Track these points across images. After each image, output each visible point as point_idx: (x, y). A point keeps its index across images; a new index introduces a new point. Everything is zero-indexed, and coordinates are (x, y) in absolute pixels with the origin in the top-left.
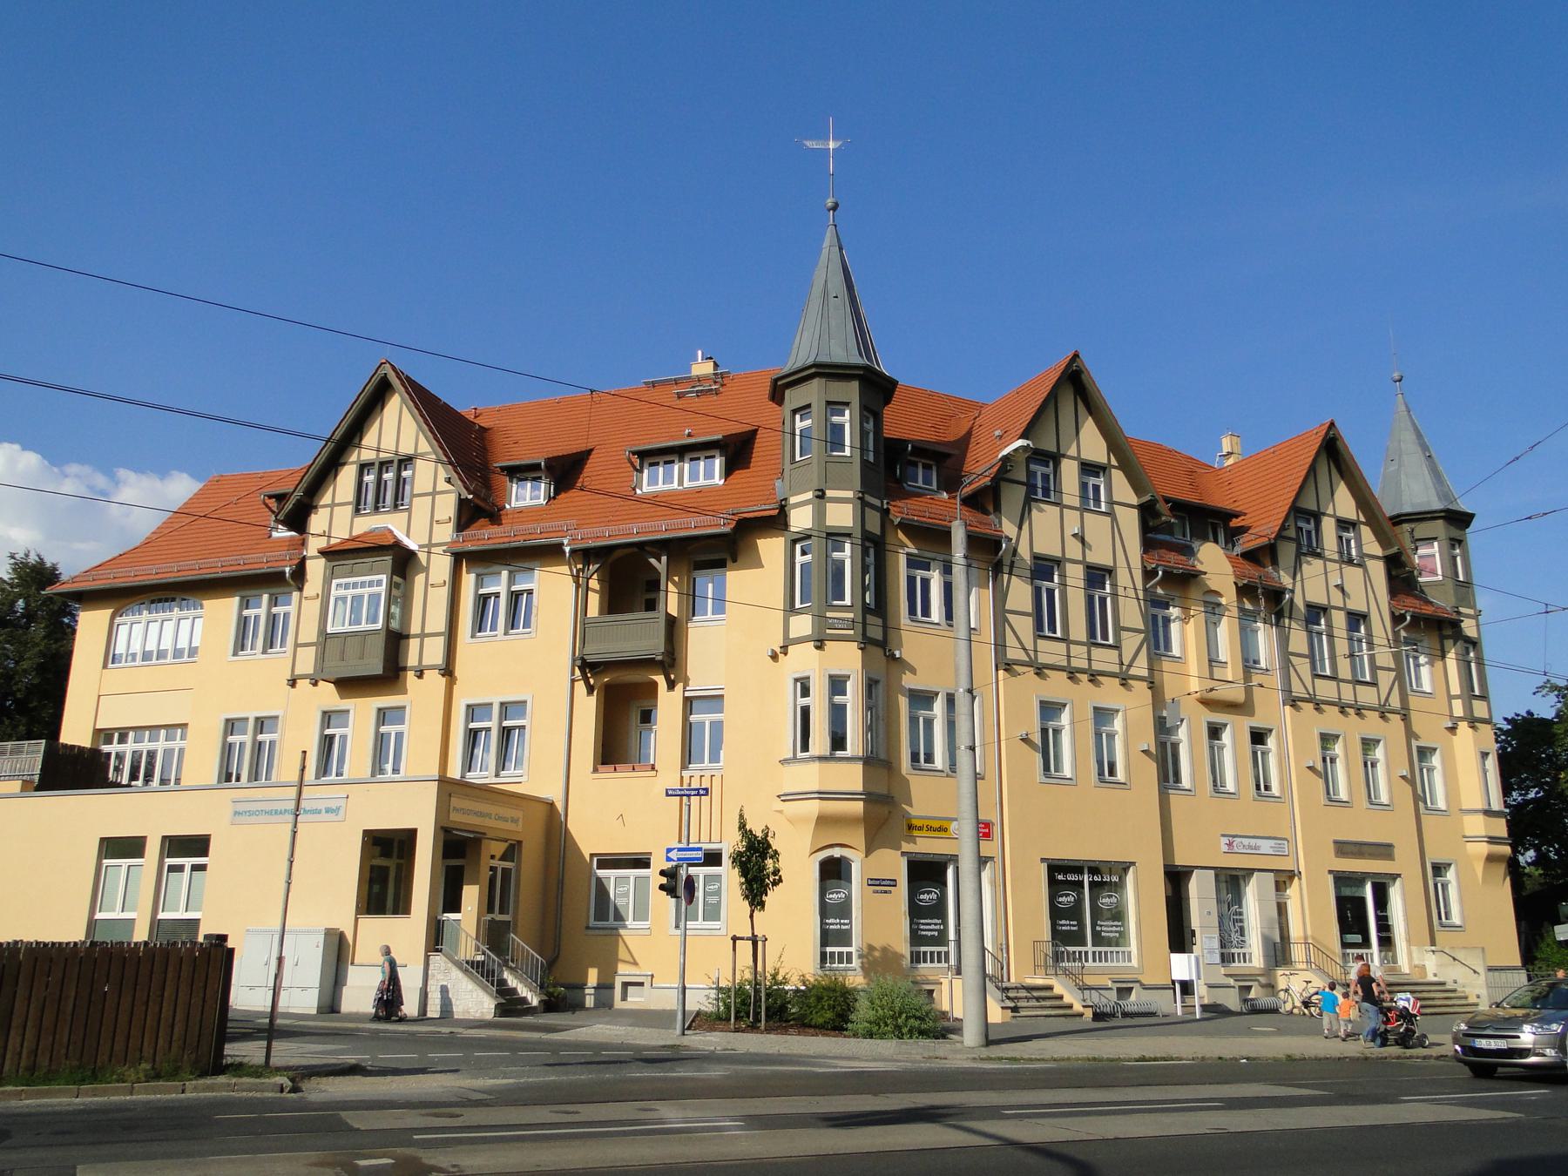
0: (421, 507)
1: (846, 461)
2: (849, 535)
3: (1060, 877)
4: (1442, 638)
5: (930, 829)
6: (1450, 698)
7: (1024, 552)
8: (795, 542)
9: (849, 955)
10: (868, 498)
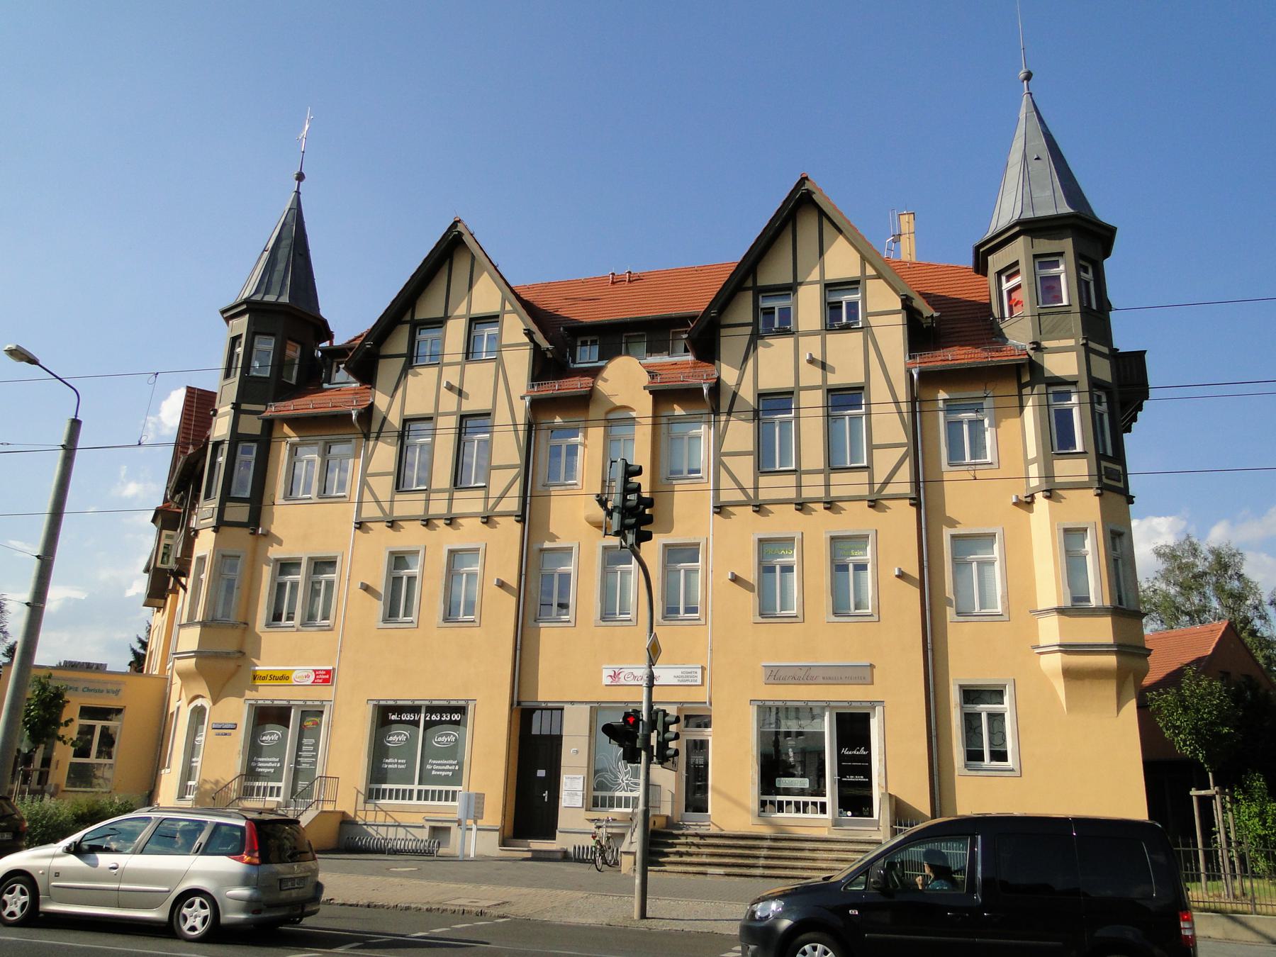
1: (1066, 311)
3: (394, 717)
4: (1021, 386)
5: (273, 678)
6: (1027, 463)
7: (747, 394)
9: (823, 805)
10: (1092, 345)
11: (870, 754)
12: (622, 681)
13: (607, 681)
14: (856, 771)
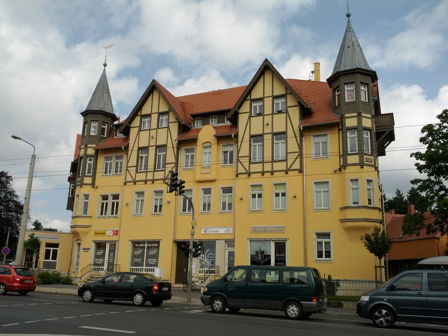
2: (356, 129)
3: (137, 246)
8: (88, 157)
11: (285, 256)
12: (208, 233)
13: (203, 233)
14: (281, 261)
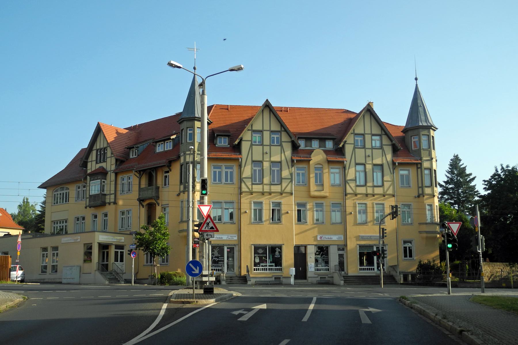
0: (109, 160)
